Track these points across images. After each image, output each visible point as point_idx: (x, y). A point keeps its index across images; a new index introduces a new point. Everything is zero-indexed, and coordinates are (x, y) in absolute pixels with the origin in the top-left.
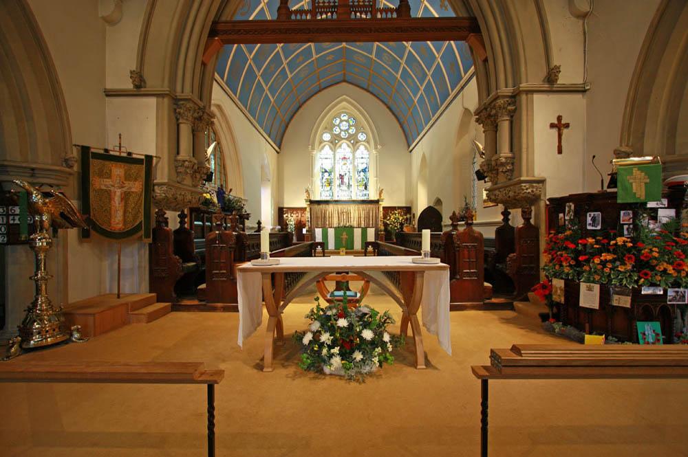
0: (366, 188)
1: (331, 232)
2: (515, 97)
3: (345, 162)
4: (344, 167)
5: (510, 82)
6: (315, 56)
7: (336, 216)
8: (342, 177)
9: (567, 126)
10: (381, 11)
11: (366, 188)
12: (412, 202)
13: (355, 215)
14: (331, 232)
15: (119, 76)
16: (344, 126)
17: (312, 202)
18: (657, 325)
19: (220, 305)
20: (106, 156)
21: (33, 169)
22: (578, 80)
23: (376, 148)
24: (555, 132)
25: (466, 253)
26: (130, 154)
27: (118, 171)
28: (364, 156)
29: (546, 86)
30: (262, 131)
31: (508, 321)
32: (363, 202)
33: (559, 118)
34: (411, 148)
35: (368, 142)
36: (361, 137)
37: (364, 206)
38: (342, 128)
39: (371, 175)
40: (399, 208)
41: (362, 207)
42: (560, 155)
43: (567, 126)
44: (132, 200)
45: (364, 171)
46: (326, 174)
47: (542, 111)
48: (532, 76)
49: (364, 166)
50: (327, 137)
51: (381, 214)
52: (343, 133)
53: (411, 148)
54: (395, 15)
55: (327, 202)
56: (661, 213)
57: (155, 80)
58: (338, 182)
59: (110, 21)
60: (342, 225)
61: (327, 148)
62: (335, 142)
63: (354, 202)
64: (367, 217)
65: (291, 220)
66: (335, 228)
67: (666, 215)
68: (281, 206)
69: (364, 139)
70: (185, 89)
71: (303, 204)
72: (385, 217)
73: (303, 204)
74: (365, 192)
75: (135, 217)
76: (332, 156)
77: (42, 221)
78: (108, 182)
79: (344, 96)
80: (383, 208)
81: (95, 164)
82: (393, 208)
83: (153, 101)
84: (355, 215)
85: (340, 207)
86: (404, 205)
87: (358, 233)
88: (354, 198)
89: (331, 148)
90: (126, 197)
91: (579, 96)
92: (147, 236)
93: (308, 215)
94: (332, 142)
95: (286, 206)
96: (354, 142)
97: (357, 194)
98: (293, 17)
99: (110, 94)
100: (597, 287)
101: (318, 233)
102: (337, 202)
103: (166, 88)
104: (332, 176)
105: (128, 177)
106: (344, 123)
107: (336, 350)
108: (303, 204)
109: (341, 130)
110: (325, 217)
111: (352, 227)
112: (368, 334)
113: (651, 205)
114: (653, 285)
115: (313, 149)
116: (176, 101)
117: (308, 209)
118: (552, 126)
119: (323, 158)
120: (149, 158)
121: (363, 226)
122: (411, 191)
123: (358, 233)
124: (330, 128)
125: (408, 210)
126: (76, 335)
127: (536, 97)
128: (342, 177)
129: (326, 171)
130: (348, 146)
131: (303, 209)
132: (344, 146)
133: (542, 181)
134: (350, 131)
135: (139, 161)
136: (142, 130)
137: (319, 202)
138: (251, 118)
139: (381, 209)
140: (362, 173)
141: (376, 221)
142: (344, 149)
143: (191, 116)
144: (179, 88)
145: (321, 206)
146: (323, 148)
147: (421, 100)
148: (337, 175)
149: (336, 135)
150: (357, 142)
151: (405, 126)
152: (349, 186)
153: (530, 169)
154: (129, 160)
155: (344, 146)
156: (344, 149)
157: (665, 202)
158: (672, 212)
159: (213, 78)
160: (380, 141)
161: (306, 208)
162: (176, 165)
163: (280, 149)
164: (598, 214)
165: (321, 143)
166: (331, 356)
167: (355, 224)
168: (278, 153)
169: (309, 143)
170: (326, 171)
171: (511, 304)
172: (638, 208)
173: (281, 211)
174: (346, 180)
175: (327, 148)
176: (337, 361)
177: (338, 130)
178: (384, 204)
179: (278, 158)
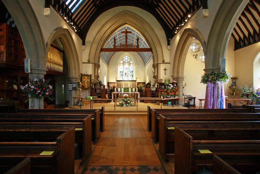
0: (133, 77)
1: (123, 89)
2: (157, 64)
3: (127, 69)
4: (126, 71)
5: (157, 62)
6: (119, 43)
7: (124, 84)
8: (126, 74)
9: (167, 70)
10: (133, 46)
11: (133, 77)
12: (145, 81)
13: (129, 85)
14: (123, 89)
15: (85, 59)
16: (127, 59)
17: (117, 81)
18: (171, 102)
19: (103, 102)
20: (84, 75)
21: (38, 70)
22: (169, 61)
23: (135, 66)
24: (164, 71)
25: (148, 93)
26: (88, 74)
27: (86, 77)
28: (132, 67)
29: (162, 63)
30: (105, 62)
31: (156, 104)
32: (132, 81)
33: (165, 68)
34: (145, 65)
35: (133, 64)
36: (131, 62)
37: (132, 82)
38: (126, 59)
39: (134, 73)
40: (142, 83)
41: (131, 82)
42: (165, 75)
43: (167, 70)
44: (88, 82)
45: (132, 72)
46: (121, 73)
47: (162, 67)
48: (160, 61)
49: (132, 70)
50: (121, 62)
51: (137, 84)
52: (126, 61)
53: (145, 65)
54: (136, 47)
55: (121, 81)
56: (171, 86)
57: (91, 61)
58: (125, 75)
59: (83, 50)
60: (126, 87)
61: (122, 65)
62: (124, 63)
63: (129, 81)
64: (133, 85)
65: (111, 85)
66: (124, 88)
67: (172, 86)
68: (108, 82)
69: (132, 63)
70: (97, 62)
71: (115, 81)
72: (138, 85)
73: (115, 81)
74: (132, 78)
75: (89, 85)
76: (123, 68)
77: (80, 87)
78: (85, 80)
79: (126, 26)
80: (138, 83)
81: (83, 76)
82: (140, 83)
83: (91, 64)
84: (129, 85)
85: (125, 82)
86: (143, 82)
87: (130, 89)
88: (129, 80)
89: (123, 65)
90: (87, 82)
91: (169, 64)
92: (90, 89)
93: (116, 84)
94: (123, 64)
95: (110, 82)
96: (129, 64)
97: (130, 78)
98: (117, 47)
99: (83, 63)
100: (163, 97)
101: (119, 89)
102: (124, 81)
103: (94, 62)
104: (123, 73)
105: (88, 78)
106: (126, 58)
107: (125, 103)
108: (115, 81)
109: (126, 60)
110: (121, 85)
111: (128, 88)
112: (129, 102)
113: (170, 85)
114: (169, 96)
115: (118, 66)
116: (95, 64)
117: (116, 83)
118: (164, 70)
119: (120, 68)
120: (91, 75)
121: (131, 88)
122: (145, 78)
123: (130, 89)
124: (122, 59)
125: (144, 83)
126: (84, 104)
127: (161, 64)
128: (126, 74)
129: (121, 72)
130: (128, 65)
131: (115, 83)
132: (127, 65)
133: (162, 80)
134: (128, 60)
135: (89, 76)
136: (88, 70)
137: (119, 81)
138: (103, 60)
139: (137, 83)
140: (131, 73)
141: (135, 87)
142: (127, 66)
143: (97, 66)
144: (95, 62)
145: (120, 82)
146: (120, 65)
147: (146, 54)
148: (125, 73)
149: (124, 61)
150: (130, 64)
151: (144, 59)
152: (128, 76)
153: (160, 78)
154: (88, 75)
155: (127, 65)
156: (127, 66)
157: (172, 84)
158: (173, 86)
159: (100, 58)
160: (137, 63)
161: (115, 83)
162: (95, 76)
163: (108, 65)
164: (163, 86)
165: (120, 64)
166: (124, 104)
167: (129, 87)
168: (108, 67)
169: (116, 64)
170: (121, 72)
171: (156, 102)
172: (168, 85)
173: (108, 83)
174: (127, 74)
175: (122, 65)
176: (125, 105)
177: (125, 60)
178: (138, 81)
179: (108, 68)
